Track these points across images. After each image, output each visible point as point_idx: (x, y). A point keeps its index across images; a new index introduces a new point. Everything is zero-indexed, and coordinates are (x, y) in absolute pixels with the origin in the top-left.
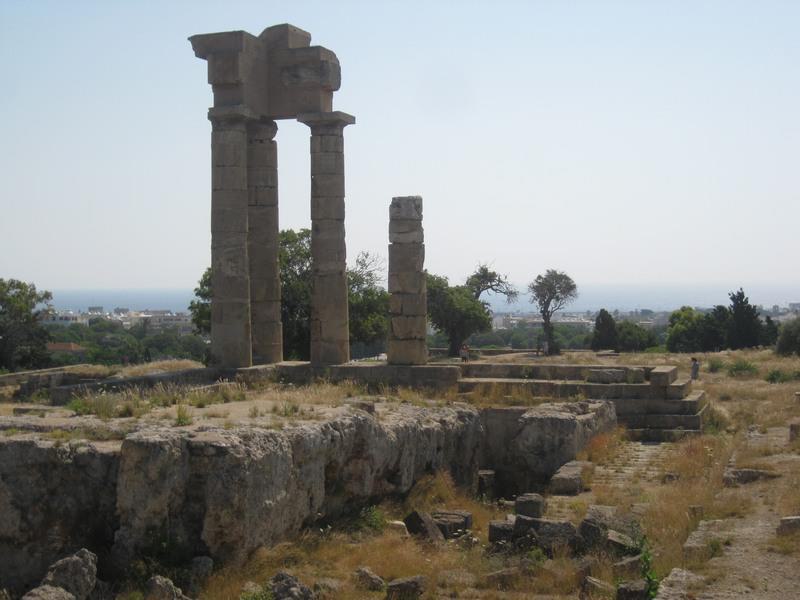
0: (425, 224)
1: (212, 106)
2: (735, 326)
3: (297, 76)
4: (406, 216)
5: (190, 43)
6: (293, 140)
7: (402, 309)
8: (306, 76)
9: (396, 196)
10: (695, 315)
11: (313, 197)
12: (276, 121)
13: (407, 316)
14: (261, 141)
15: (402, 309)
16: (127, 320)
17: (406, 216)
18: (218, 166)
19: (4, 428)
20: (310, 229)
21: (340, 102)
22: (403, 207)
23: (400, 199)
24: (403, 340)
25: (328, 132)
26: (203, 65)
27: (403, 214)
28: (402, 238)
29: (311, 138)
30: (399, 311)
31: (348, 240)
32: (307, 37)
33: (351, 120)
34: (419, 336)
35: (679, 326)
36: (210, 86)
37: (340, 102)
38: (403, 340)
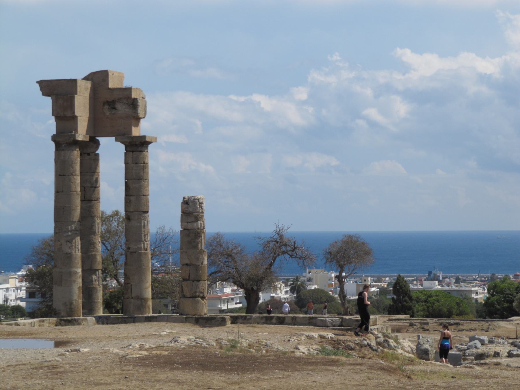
4: (191, 210)
5: (38, 85)
6: (111, 154)
7: (189, 276)
8: (122, 108)
11: (126, 195)
12: (97, 138)
13: (193, 281)
14: (89, 154)
15: (189, 276)
17: (191, 210)
18: (60, 175)
19: (518, 356)
20: (133, 128)
22: (190, 204)
24: (190, 297)
25: (136, 148)
27: (191, 209)
28: (190, 226)
29: (125, 153)
30: (188, 278)
32: (116, 140)
34: (201, 295)
36: (54, 117)
38: (190, 297)
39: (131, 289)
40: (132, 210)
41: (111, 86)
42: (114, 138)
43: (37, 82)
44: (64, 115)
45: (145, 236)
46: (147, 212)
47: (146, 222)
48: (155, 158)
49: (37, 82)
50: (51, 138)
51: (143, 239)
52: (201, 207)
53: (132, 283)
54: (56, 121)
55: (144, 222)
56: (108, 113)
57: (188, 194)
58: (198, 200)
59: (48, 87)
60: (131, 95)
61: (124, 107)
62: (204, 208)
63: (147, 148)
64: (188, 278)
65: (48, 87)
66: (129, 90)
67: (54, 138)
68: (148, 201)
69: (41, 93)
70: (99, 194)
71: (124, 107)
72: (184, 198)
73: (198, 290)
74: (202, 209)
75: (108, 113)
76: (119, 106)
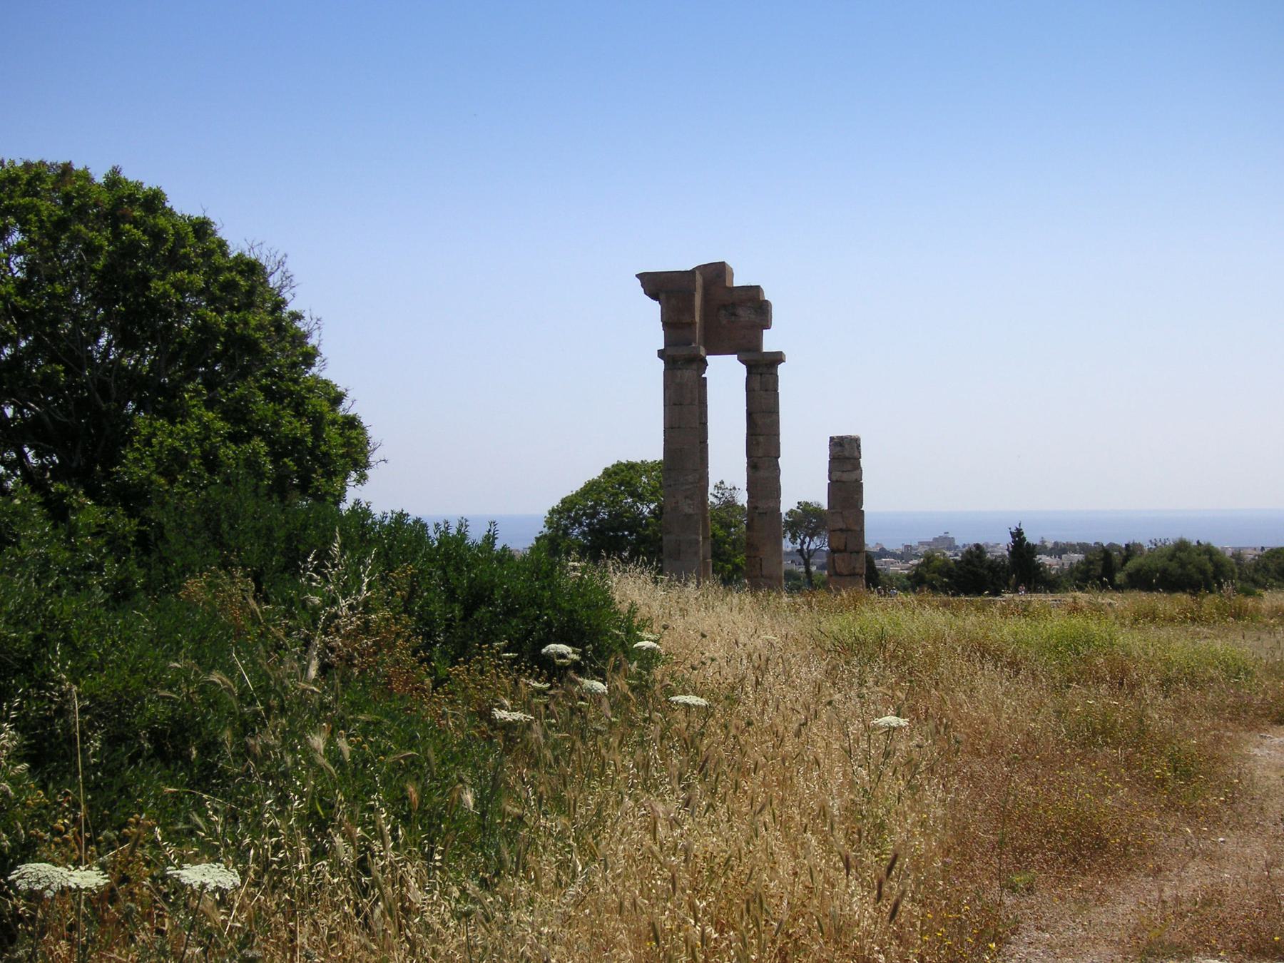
0: (864, 462)
1: (662, 347)
2: (1185, 573)
3: (734, 314)
4: (845, 454)
5: (638, 281)
6: (725, 377)
8: (745, 315)
9: (835, 434)
10: (518, 558)
16: (1249, 556)
17: (845, 454)
21: (770, 342)
23: (842, 438)
25: (763, 373)
26: (655, 307)
31: (784, 480)
33: (115, 171)
35: (1173, 566)
37: (770, 342)
43: (657, 285)
49: (657, 285)
72: (832, 439)
76: (741, 312)
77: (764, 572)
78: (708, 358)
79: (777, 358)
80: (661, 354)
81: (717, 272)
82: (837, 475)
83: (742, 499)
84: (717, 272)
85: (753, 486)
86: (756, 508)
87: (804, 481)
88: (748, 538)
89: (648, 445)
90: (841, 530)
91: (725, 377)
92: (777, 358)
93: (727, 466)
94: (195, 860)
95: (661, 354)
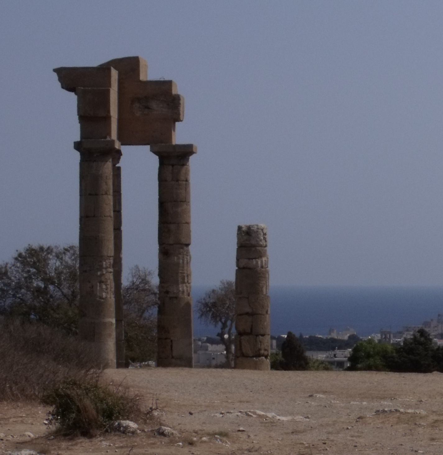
3: (148, 108)
4: (249, 244)
6: (138, 166)
8: (158, 108)
17: (249, 244)
21: (181, 135)
25: (174, 161)
26: (72, 99)
37: (181, 135)
39: (172, 347)
40: (171, 242)
41: (142, 78)
42: (148, 147)
43: (55, 70)
44: (92, 117)
45: (188, 276)
46: (188, 245)
47: (188, 257)
48: (198, 172)
49: (55, 70)
50: (73, 145)
51: (186, 281)
52: (265, 238)
53: (172, 338)
54: (80, 122)
55: (187, 258)
56: (138, 114)
57: (245, 223)
58: (262, 230)
59: (70, 78)
60: (171, 90)
61: (161, 106)
62: (268, 239)
63: (188, 160)
64: (249, 331)
65: (70, 78)
66: (169, 84)
67: (121, 155)
68: (189, 231)
69: (59, 84)
70: (189, 217)
71: (161, 106)
72: (240, 228)
73: (263, 346)
74: (266, 241)
75: (138, 114)
76: (154, 105)
77: (175, 354)
78: (126, 150)
79: (186, 152)
80: (78, 146)
81: (129, 66)
82: (244, 262)
83: (155, 281)
84: (129, 66)
85: (162, 273)
86: (167, 292)
87: (210, 268)
88: (159, 321)
89: (62, 231)
90: (247, 314)
91: (138, 166)
92: (186, 152)
93: (139, 252)
94: (125, 420)
95: (78, 146)
